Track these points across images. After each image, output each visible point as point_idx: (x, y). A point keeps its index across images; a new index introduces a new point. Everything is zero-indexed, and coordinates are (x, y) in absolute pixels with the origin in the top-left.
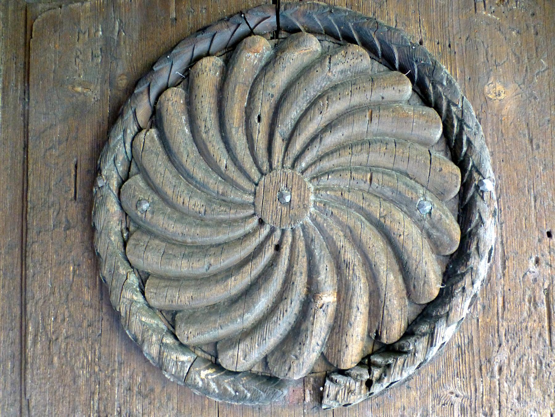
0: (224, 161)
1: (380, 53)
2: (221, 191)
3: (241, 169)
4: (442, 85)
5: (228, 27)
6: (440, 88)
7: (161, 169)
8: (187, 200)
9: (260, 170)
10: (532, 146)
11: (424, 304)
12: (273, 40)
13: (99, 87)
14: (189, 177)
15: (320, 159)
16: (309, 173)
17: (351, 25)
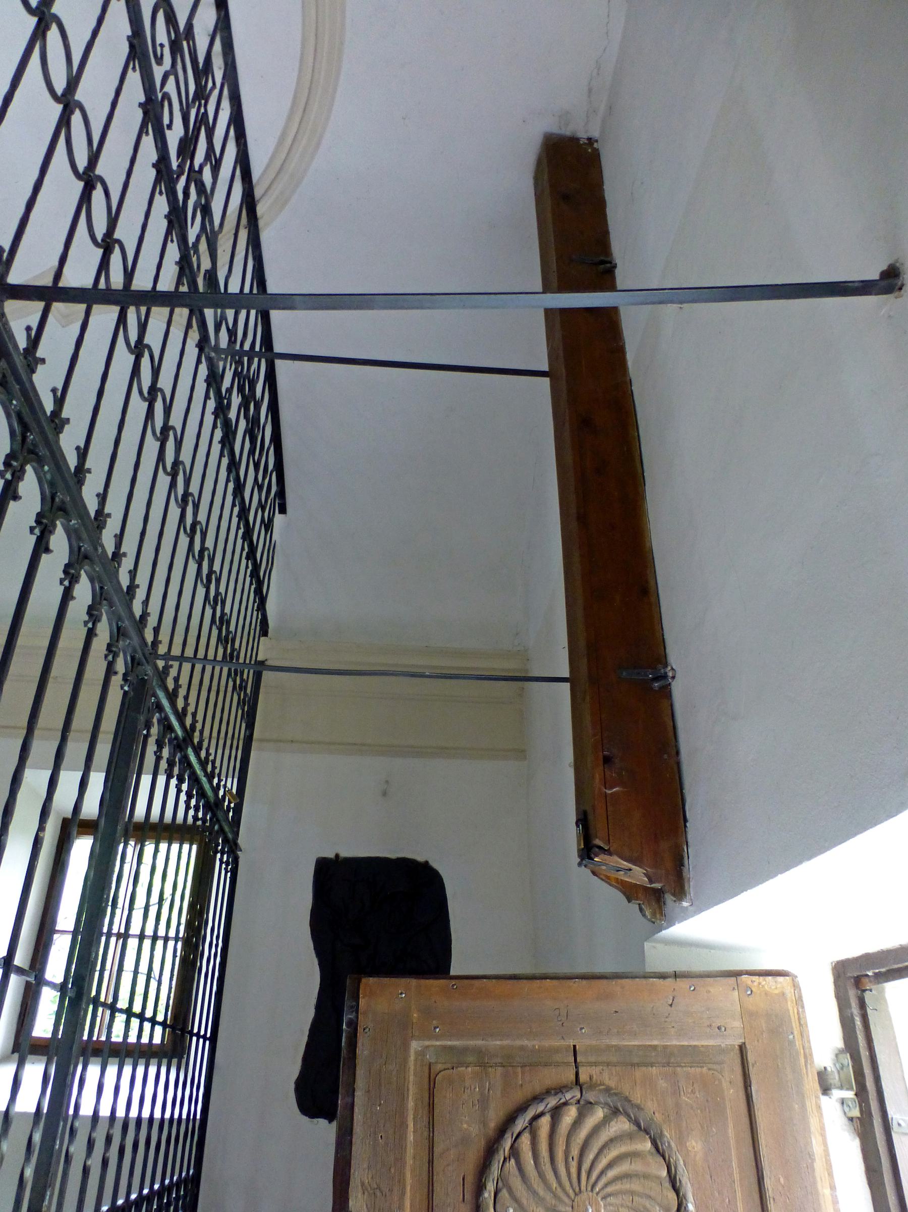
0: (555, 1185)
1: (633, 1119)
2: (553, 1204)
3: (564, 1190)
4: (665, 1145)
5: (555, 1099)
6: (664, 1147)
7: (520, 1187)
8: (535, 1208)
9: (574, 1191)
10: (712, 1180)
11: (651, 1147)
12: (577, 1105)
13: (477, 1126)
14: (535, 1193)
15: (606, 1185)
16: (601, 1194)
17: (619, 1105)
